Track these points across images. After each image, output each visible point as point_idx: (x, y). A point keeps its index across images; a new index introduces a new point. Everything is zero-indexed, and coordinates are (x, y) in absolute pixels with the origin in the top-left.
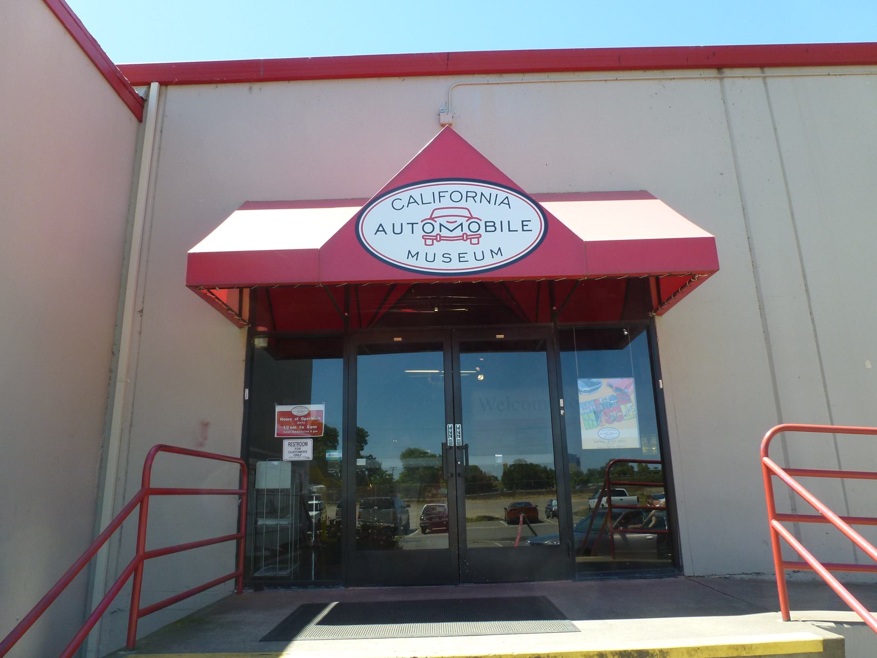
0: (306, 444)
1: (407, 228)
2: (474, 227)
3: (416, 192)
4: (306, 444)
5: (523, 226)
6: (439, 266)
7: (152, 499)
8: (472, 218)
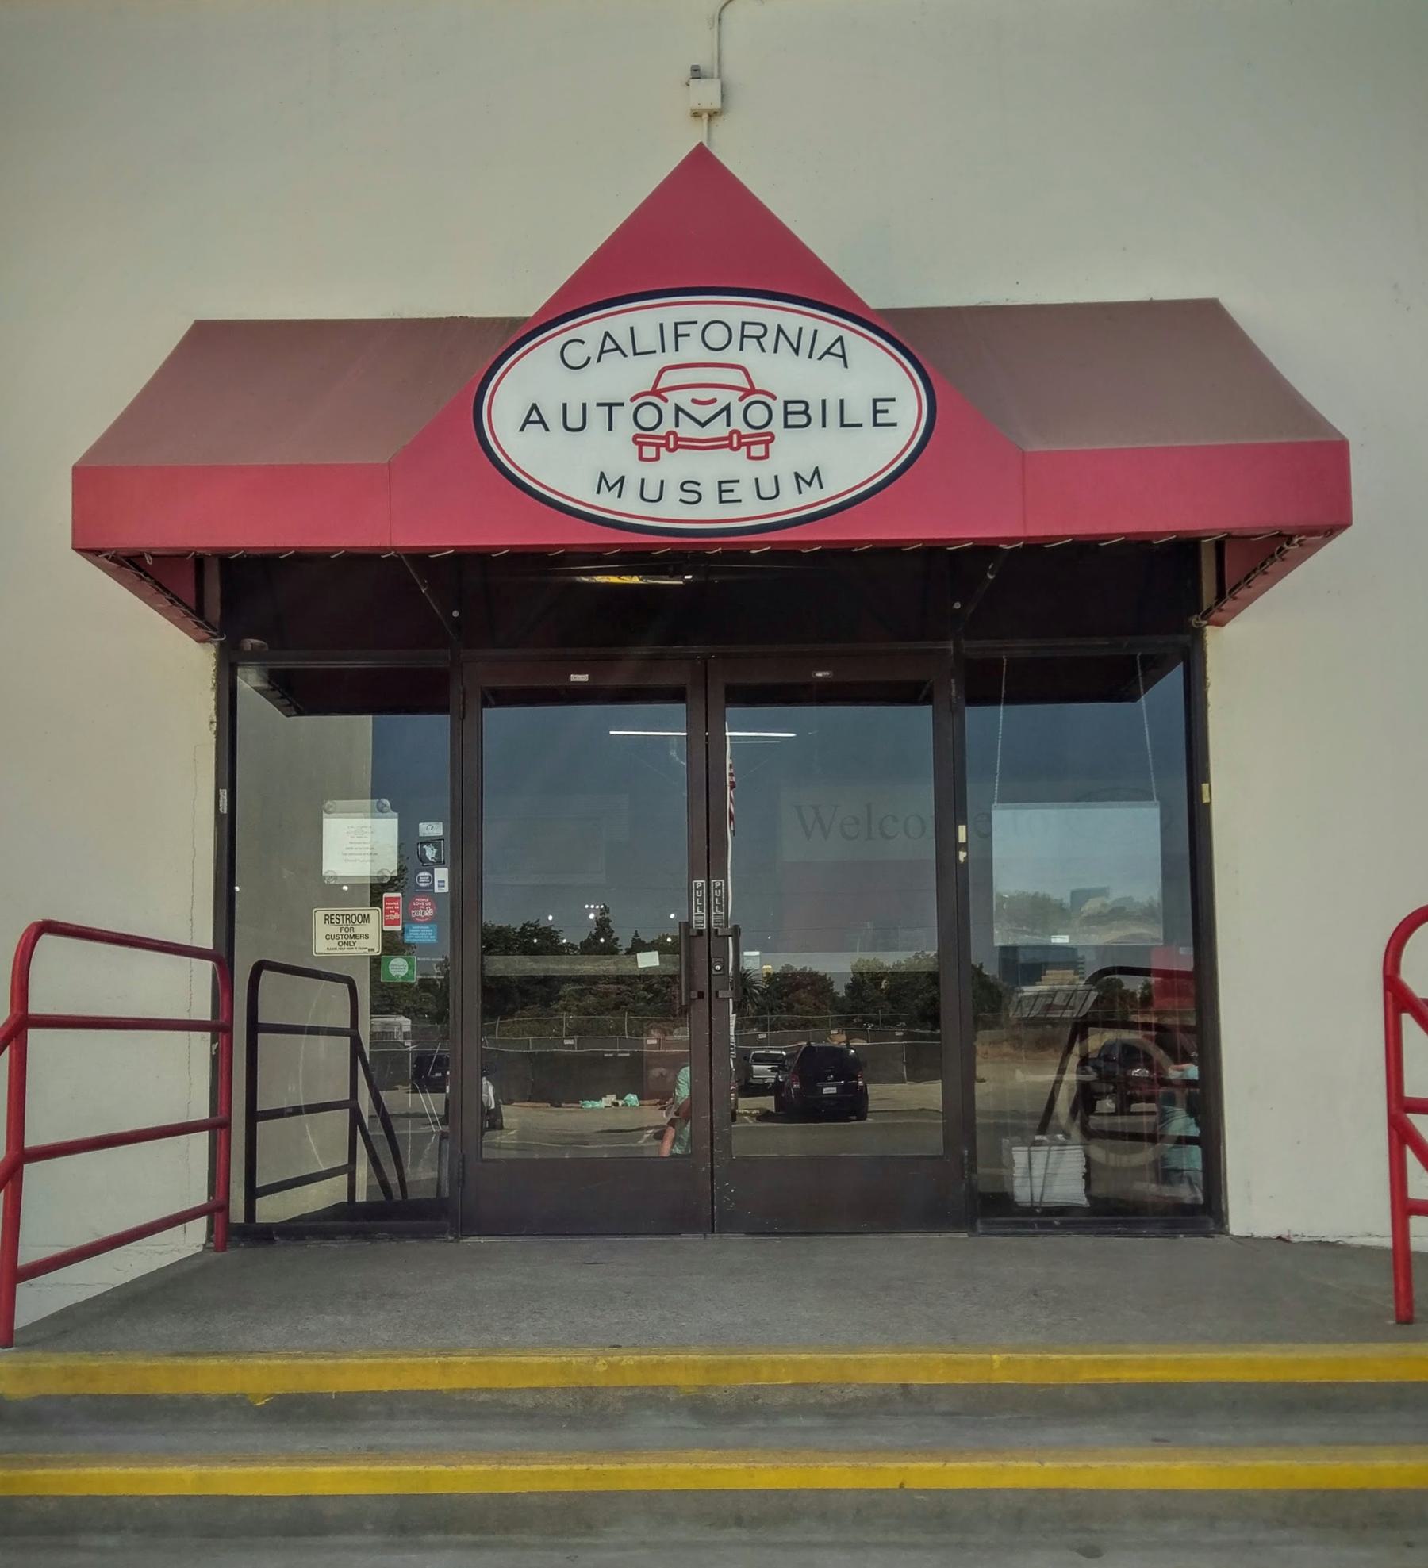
0: (366, 919)
1: (598, 416)
2: (758, 415)
3: (619, 322)
4: (366, 919)
5: (876, 412)
6: (672, 511)
7: (34, 1035)
8: (752, 391)
